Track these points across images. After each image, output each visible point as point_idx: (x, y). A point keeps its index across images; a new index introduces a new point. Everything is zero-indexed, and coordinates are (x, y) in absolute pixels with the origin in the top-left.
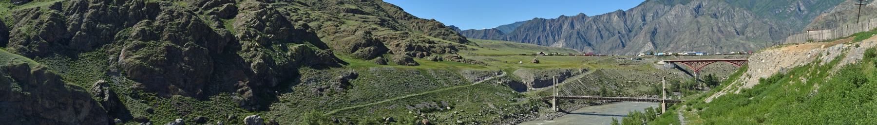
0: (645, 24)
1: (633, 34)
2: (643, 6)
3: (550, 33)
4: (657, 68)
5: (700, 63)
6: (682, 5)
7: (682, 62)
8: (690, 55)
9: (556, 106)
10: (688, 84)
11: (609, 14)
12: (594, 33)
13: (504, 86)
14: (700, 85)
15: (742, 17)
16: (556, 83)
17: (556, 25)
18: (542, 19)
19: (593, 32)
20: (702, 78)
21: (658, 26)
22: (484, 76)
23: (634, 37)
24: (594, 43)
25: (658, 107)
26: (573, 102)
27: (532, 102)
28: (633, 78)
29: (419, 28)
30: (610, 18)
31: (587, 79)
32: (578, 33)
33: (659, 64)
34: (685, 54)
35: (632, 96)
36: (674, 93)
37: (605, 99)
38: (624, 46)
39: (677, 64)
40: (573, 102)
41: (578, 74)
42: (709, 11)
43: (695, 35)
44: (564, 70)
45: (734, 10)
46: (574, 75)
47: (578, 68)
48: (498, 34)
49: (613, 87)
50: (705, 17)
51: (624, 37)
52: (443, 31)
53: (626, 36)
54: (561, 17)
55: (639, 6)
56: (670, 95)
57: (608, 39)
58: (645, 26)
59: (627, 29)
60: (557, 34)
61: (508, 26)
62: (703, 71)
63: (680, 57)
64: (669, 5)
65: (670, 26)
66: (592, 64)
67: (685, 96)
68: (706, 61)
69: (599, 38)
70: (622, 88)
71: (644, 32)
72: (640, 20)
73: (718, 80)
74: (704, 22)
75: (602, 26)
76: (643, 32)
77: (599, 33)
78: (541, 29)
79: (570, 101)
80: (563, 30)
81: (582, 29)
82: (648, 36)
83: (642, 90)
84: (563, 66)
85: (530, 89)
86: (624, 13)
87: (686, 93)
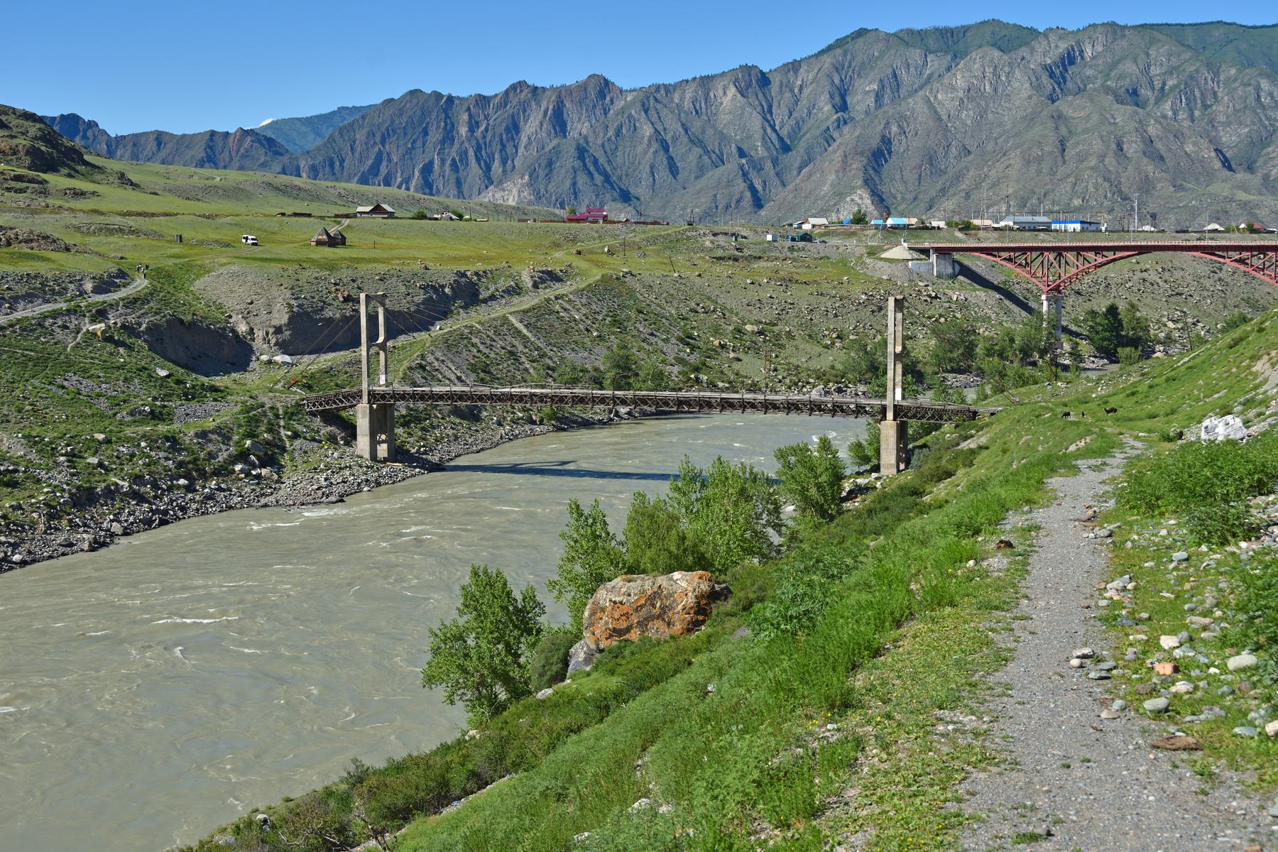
0: (845, 123)
1: (795, 157)
2: (839, 51)
3: (471, 153)
4: (877, 275)
5: (1070, 256)
6: (996, 54)
9: (373, 435)
10: (1012, 340)
11: (705, 82)
13: (119, 344)
14: (1067, 347)
15: (1251, 100)
16: (373, 336)
17: (498, 119)
18: (438, 95)
19: (640, 149)
20: (1076, 321)
21: (894, 129)
22: (16, 299)
23: (800, 169)
24: (641, 190)
25: (864, 438)
26: (472, 416)
27: (253, 417)
28: (768, 314)
31: (552, 312)
32: (581, 152)
33: (886, 260)
34: (1002, 224)
35: (754, 388)
36: (950, 376)
37: (624, 402)
38: (758, 203)
39: (966, 262)
40: (472, 416)
41: (515, 291)
42: (1107, 77)
43: (1045, 167)
44: (445, 274)
45: (1217, 74)
47: (516, 268)
49: (672, 350)
50: (1091, 101)
51: (760, 169)
53: (768, 165)
54: (514, 87)
55: (822, 52)
56: (930, 388)
57: (697, 178)
58: (846, 129)
59: (774, 136)
60: (497, 156)
61: (309, 121)
62: (1078, 293)
63: (981, 234)
64: (946, 53)
65: (946, 129)
66: (591, 252)
67: (1000, 390)
68: (1098, 250)
69: (663, 174)
70: (712, 353)
71: (840, 153)
72: (827, 108)
73: (1146, 329)
74: (1088, 118)
76: (835, 154)
78: (435, 136)
79: (457, 412)
80: (524, 140)
81: (596, 135)
82: (857, 165)
84: (441, 259)
85: (264, 358)
86: (764, 80)
87: (1002, 376)
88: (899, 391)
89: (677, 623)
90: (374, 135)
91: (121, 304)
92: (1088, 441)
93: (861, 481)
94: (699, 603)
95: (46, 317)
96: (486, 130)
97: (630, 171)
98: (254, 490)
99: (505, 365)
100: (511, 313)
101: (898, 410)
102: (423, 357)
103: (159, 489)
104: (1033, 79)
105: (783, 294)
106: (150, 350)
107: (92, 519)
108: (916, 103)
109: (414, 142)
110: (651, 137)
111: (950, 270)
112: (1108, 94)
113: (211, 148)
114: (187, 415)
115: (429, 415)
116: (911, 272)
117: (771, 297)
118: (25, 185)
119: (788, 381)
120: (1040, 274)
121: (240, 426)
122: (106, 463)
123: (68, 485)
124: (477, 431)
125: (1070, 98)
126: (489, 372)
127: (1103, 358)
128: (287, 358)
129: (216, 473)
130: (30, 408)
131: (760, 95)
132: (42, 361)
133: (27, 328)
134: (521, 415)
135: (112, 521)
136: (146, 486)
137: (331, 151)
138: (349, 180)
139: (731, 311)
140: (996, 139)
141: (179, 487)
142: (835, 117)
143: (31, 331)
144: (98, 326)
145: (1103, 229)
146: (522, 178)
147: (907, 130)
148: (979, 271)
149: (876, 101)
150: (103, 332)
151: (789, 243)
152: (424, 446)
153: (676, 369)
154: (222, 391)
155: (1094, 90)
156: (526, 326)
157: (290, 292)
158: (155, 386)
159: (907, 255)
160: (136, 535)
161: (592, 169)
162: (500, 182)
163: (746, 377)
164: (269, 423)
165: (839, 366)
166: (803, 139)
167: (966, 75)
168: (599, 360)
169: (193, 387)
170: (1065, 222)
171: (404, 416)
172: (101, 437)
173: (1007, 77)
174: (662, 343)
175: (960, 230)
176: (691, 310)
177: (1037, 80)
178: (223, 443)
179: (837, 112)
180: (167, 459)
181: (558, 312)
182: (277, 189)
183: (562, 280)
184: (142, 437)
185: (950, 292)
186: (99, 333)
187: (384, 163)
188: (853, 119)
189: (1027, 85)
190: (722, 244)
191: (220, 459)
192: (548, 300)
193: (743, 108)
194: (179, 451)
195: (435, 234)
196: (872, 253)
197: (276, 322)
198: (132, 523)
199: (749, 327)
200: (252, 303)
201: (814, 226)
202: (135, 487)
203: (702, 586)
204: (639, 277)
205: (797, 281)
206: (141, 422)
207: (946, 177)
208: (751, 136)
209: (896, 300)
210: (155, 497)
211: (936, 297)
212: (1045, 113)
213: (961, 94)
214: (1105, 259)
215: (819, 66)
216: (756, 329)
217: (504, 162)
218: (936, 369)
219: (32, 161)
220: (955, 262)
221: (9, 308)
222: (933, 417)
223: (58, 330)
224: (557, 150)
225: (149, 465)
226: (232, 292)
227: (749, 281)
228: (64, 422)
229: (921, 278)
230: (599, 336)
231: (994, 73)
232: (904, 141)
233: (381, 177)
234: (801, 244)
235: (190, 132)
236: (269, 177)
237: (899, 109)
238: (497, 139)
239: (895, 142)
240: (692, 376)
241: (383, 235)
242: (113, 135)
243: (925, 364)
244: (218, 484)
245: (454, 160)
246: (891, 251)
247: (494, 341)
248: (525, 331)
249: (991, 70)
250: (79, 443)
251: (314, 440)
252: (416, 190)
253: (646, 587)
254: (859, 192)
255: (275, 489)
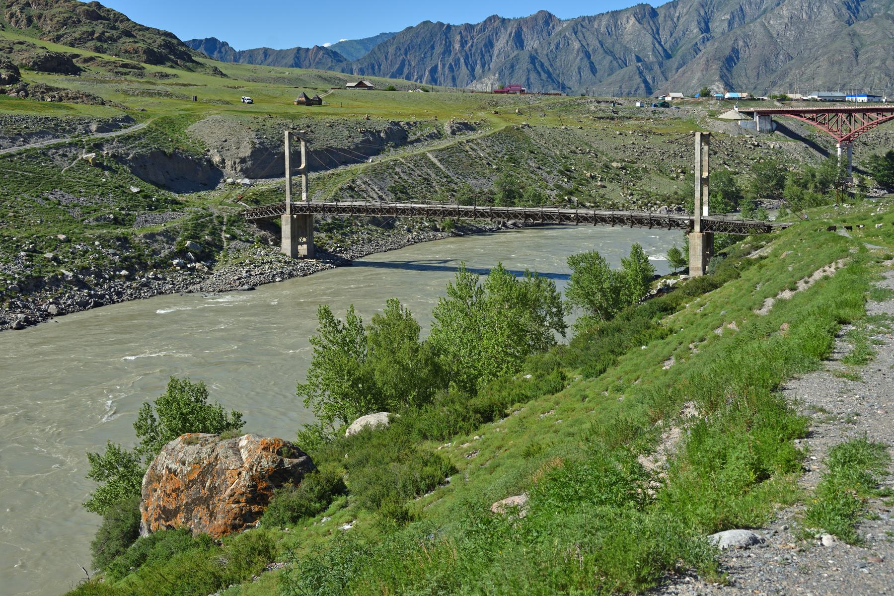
0: (708, 40)
1: (674, 62)
3: (462, 60)
5: (858, 116)
7: (797, 113)
8: (824, 100)
10: (814, 176)
11: (615, 14)
12: (572, 59)
13: (104, 168)
14: (856, 181)
17: (479, 39)
18: (441, 24)
19: (571, 57)
20: (863, 163)
21: (741, 43)
28: (628, 156)
29: (29, 21)
30: (616, 25)
32: (533, 59)
33: (722, 120)
35: (614, 207)
36: (765, 201)
39: (781, 121)
41: (438, 136)
43: (844, 67)
46: (418, 140)
48: (329, 60)
51: (650, 69)
52: (99, 29)
53: (656, 67)
54: (490, 19)
57: (609, 75)
58: (708, 44)
59: (660, 49)
60: (479, 62)
61: (362, 42)
62: (865, 144)
63: (793, 103)
65: (776, 43)
66: (506, 113)
68: (879, 111)
69: (586, 73)
71: (704, 58)
72: (696, 30)
74: (874, 35)
75: (593, 42)
76: (701, 58)
77: (586, 61)
78: (439, 49)
79: (374, 221)
82: (715, 66)
83: (653, 189)
85: (230, 180)
86: (654, 13)
88: (706, 209)
89: (219, 516)
90: (400, 49)
91: (116, 140)
92: (840, 265)
93: (671, 282)
94: (255, 487)
95: (51, 148)
96: (472, 45)
97: (565, 71)
98: (186, 279)
99: (419, 188)
100: (429, 152)
101: (704, 224)
102: (353, 181)
103: (102, 278)
104: (836, 10)
105: (642, 142)
106: (132, 173)
107: (33, 302)
108: (755, 26)
109: (426, 53)
110: (578, 49)
111: (769, 127)
112: (888, 19)
113: (298, 58)
114: (146, 221)
115: (351, 224)
116: (740, 128)
117: (633, 144)
118: (128, 70)
119: (640, 202)
120: (835, 129)
121: (186, 230)
122: (61, 257)
123: (19, 274)
124: (389, 236)
125: (861, 22)
126: (406, 193)
127: (883, 189)
128: (247, 181)
129: (156, 266)
130: (13, 214)
131: (651, 23)
132: (36, 181)
133: (32, 156)
134: (427, 224)
135: (51, 303)
136: (90, 276)
137: (373, 59)
138: (384, 76)
139: (602, 153)
140: (810, 49)
141: (120, 277)
142: (701, 36)
143: (35, 158)
144: (89, 155)
145: (884, 100)
146: (494, 76)
147: (749, 44)
148: (790, 127)
149: (729, 26)
150: (93, 159)
151: (653, 108)
152: (340, 247)
153: (554, 193)
154: (181, 204)
155: (879, 17)
156: (440, 161)
157: (255, 134)
158: (125, 200)
159: (738, 116)
160: (69, 315)
161: (540, 69)
162: (480, 78)
163: (608, 199)
164: (213, 228)
165: (680, 193)
166: (680, 50)
167: (790, 8)
168: (492, 185)
169: (158, 200)
170: (855, 96)
171: (329, 224)
172: (62, 237)
173: (818, 9)
174: (546, 174)
175: (778, 101)
176: (571, 152)
177: (839, 11)
178: (167, 243)
179: (702, 33)
180: (115, 254)
181: (467, 151)
182: (325, 79)
183: (475, 130)
184: (97, 237)
185: (769, 142)
186: (90, 161)
187: (406, 67)
188: (713, 37)
189: (832, 14)
190: (603, 108)
191: (162, 255)
192: (460, 143)
193: (639, 31)
194: (127, 249)
195: (394, 100)
196: (712, 115)
197: (242, 155)
198: (69, 305)
199: (614, 164)
200: (226, 141)
201: (673, 98)
202: (81, 276)
203: (264, 463)
204: (534, 128)
205: (654, 133)
206: (103, 227)
207: (776, 74)
208: (645, 49)
209: (702, 135)
210: (96, 285)
211: (758, 145)
212: (844, 32)
213: (786, 20)
214: (884, 118)
215: (690, 4)
216: (619, 165)
217: (483, 66)
218: (756, 196)
219: (147, 57)
220: (772, 121)
221: (23, 141)
222: (733, 230)
223: (58, 158)
224: (517, 58)
225: (98, 259)
226: (212, 133)
227: (618, 133)
228: (38, 225)
229: (747, 132)
230: (497, 169)
231: (809, 7)
232: (747, 51)
233: (404, 75)
234: (661, 109)
235: (285, 48)
236: (322, 72)
237: (743, 30)
238: (479, 51)
239: (741, 52)
240: (566, 198)
241: (356, 100)
242: (237, 50)
243: (747, 192)
244: (155, 274)
245: (451, 64)
246: (725, 114)
247: (413, 170)
248: (438, 164)
249: (807, 4)
250: (42, 241)
251: (248, 241)
252: (427, 83)
253: (204, 455)
254: (717, 84)
255: (203, 279)
